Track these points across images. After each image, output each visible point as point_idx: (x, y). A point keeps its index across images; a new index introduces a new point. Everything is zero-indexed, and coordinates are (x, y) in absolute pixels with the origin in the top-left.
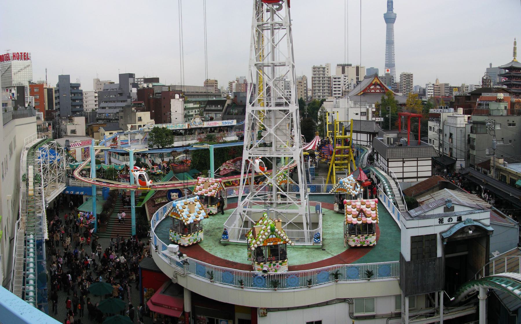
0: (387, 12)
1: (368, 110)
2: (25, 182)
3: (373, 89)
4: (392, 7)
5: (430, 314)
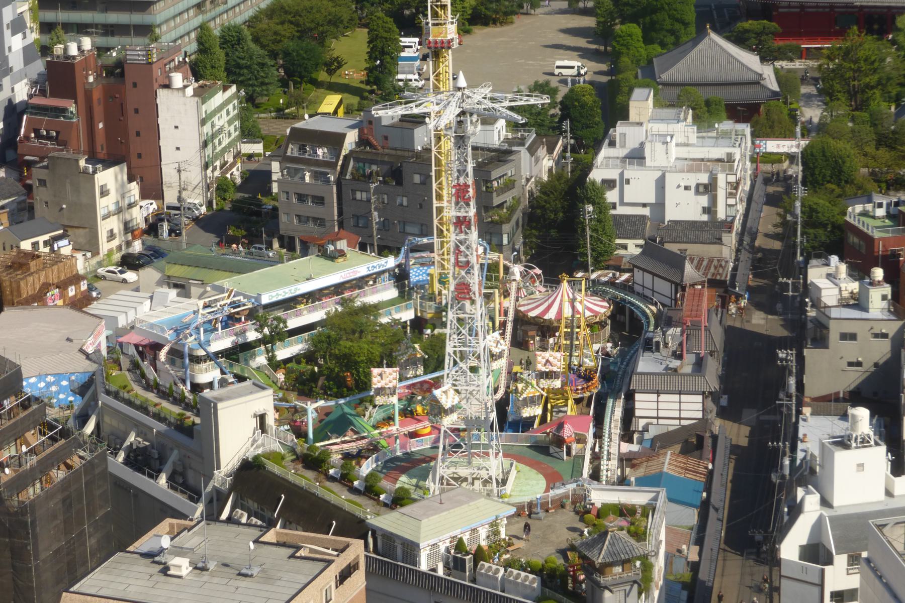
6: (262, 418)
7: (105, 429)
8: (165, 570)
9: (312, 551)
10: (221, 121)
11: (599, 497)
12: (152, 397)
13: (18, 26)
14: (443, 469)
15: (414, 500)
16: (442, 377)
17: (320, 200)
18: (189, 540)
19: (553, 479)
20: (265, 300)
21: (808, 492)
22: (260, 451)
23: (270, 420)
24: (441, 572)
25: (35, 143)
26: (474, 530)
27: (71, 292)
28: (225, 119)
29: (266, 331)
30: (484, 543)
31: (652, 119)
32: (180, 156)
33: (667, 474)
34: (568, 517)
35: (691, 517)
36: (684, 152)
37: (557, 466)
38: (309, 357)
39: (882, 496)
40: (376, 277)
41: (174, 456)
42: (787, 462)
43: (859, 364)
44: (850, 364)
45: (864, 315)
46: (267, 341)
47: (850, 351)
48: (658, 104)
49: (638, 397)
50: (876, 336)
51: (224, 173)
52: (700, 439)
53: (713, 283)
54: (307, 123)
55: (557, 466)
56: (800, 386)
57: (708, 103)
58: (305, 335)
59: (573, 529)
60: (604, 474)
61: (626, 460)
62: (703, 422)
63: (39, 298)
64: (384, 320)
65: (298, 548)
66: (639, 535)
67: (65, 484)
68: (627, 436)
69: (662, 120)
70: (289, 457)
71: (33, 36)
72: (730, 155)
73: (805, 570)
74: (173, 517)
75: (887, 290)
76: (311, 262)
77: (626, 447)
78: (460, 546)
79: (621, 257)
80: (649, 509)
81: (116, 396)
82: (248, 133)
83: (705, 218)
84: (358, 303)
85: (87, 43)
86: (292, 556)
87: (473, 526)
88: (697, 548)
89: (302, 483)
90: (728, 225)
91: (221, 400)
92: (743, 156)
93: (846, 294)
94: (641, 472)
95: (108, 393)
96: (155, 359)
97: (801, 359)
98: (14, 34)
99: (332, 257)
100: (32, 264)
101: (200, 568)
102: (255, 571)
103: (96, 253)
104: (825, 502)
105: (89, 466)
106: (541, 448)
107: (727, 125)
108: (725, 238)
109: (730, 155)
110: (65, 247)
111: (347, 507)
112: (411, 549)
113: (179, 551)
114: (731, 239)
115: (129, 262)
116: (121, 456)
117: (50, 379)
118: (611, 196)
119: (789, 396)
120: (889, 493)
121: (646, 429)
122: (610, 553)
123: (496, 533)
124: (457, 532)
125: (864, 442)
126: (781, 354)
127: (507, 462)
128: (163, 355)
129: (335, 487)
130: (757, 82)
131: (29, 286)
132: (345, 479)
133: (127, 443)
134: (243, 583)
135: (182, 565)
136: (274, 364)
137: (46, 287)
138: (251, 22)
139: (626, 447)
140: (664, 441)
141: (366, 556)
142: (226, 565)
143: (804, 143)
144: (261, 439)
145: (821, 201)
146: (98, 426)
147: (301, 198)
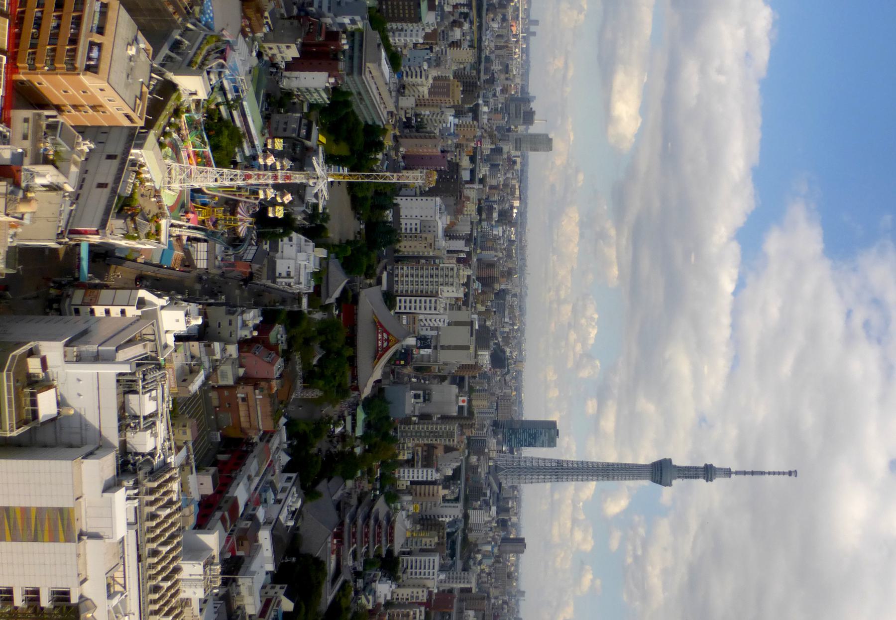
0: (675, 466)
1: (292, 278)
2: (122, 559)
3: (383, 337)
4: (686, 477)
5: (74, 217)
6: (195, 94)
7: (189, 32)
8: (129, 44)
9: (139, 105)
10: (315, 95)
11: (164, 223)
12: (204, 52)
13: (353, 22)
14: (175, 165)
15: (161, 150)
16: (212, 166)
17: (285, 130)
18: (143, 56)
19: (171, 209)
20: (245, 103)
21: (167, 301)
22: (181, 92)
23: (195, 97)
24: (130, 157)
25: (308, 23)
26: (149, 172)
27: (248, 29)
28: (317, 98)
29: (232, 102)
30: (143, 176)
31: (315, 257)
32: (302, 79)
33: (173, 253)
34: (155, 210)
35: (156, 261)
36: (303, 267)
37: (176, 211)
38: (221, 119)
39: (166, 329)
40: (253, 146)
41: (179, 58)
42: (179, 297)
43: (219, 327)
44: (219, 323)
45: (239, 329)
46: (227, 103)
47: (224, 323)
48: (321, 259)
49: (206, 244)
50: (231, 333)
51: (296, 95)
52: (188, 266)
53: (251, 274)
54: (315, 129)
55: (176, 211)
56: (210, 305)
57: (321, 278)
58: (230, 118)
59: (150, 211)
60: (173, 229)
61: (179, 238)
62: (195, 268)
63: (245, 16)
64: (236, 150)
65: (140, 99)
66: (148, 236)
67: (166, 10)
68: (189, 239)
69: (315, 259)
70: (179, 103)
71: (349, 28)
72: (301, 283)
73: (135, 299)
74: (154, 51)
75: (249, 337)
76: (260, 121)
77: (185, 238)
78: (142, 166)
79: (262, 242)
80: (159, 241)
81: (204, 38)
82: (312, 106)
83: (277, 275)
84: (243, 140)
85: (346, 47)
86: (136, 97)
87: (151, 172)
88: (143, 262)
89: (168, 107)
90: (274, 282)
91: (203, 78)
92: (300, 289)
93: (247, 322)
94: (175, 243)
95: (206, 35)
96: (221, 58)
97: (222, 304)
98: (350, 20)
99: (262, 132)
100: (259, 15)
101: (131, 58)
102: (130, 80)
103: (264, 42)
104: (163, 308)
105: (174, 22)
106: (183, 206)
107: (313, 284)
108: (270, 281)
109: (301, 283)
110: (266, 29)
111: (158, 123)
112: (140, 146)
113: (138, 51)
114: (269, 283)
115: (260, 55)
116: (178, 37)
117: (211, 15)
118: (286, 239)
119: (207, 300)
120: (167, 332)
121: (192, 246)
122: (140, 223)
123: (148, 181)
124: (148, 165)
125: (188, 322)
126: (223, 297)
127: (178, 191)
128: (222, 61)
129: (166, 120)
130: (328, 296)
131: (251, 13)
132: (169, 124)
133: (184, 40)
134: (125, 75)
135: (132, 51)
136: (218, 105)
137: (249, 19)
138: (353, 112)
139: (185, 238)
140: (187, 253)
141: (136, 127)
142: (132, 69)
143: (306, 311)
144: (187, 93)
145: (283, 316)
146: (191, 30)
147: (286, 123)
